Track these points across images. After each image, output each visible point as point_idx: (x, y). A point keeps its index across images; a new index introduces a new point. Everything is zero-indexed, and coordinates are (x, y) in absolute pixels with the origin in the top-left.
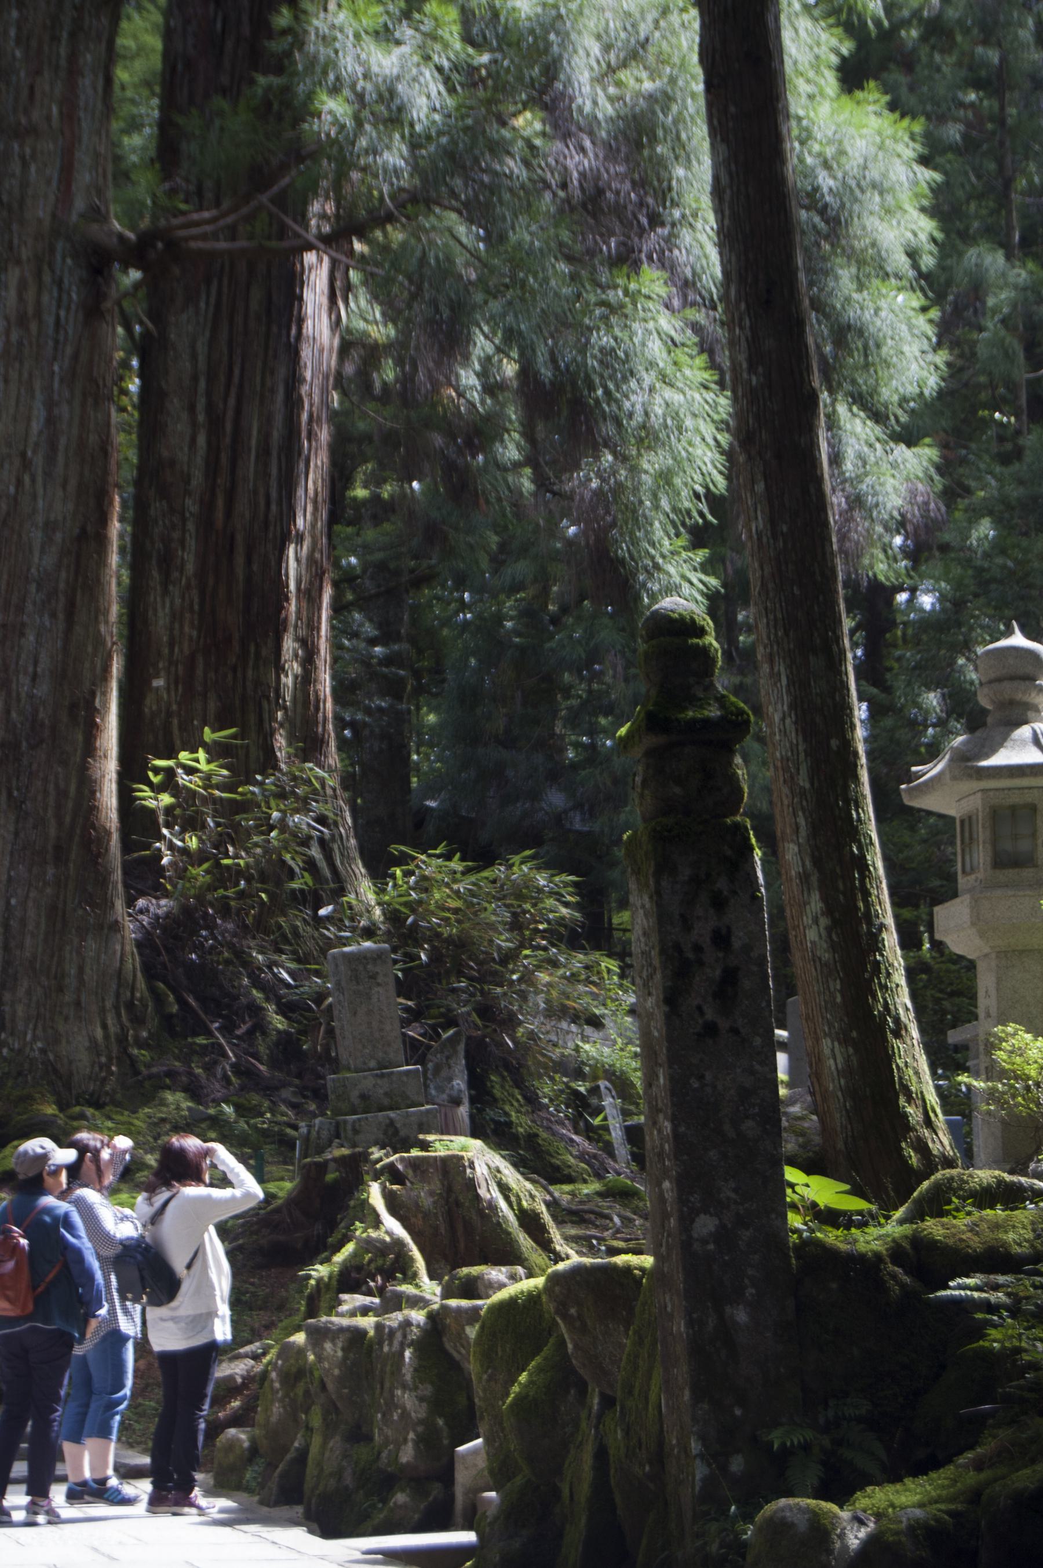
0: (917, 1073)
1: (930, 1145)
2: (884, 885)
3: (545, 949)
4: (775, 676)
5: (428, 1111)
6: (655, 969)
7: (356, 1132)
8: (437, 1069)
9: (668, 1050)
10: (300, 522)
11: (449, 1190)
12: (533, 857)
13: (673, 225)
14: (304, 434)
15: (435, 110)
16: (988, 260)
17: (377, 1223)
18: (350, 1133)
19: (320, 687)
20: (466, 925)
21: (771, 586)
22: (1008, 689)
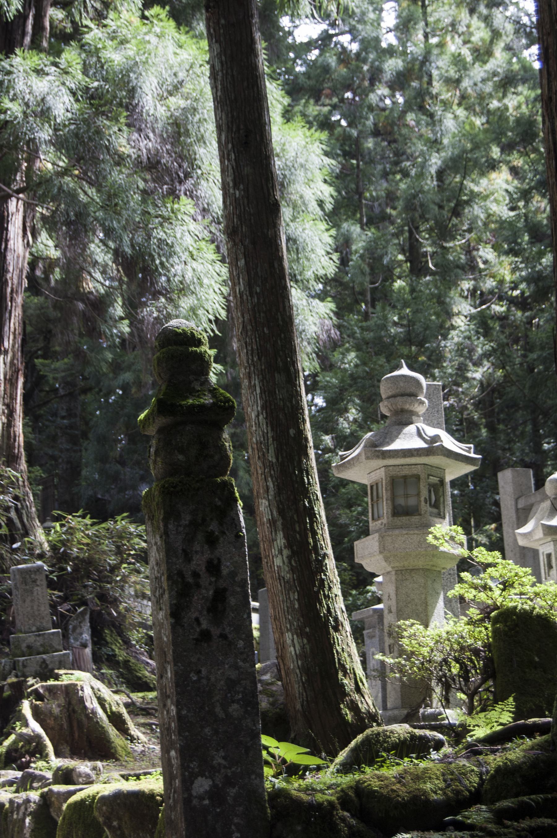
0: (350, 656)
1: (360, 705)
2: (326, 527)
3: (134, 564)
4: (252, 387)
5: (64, 654)
6: (164, 591)
7: (24, 666)
8: (75, 629)
9: (174, 652)
10: (6, 344)
11: (69, 703)
12: (127, 517)
13: (198, 178)
14: (8, 299)
15: (68, 111)
16: (353, 228)
17: (27, 725)
18: (21, 667)
19: (16, 429)
20: (92, 552)
21: (249, 327)
22: (400, 402)
